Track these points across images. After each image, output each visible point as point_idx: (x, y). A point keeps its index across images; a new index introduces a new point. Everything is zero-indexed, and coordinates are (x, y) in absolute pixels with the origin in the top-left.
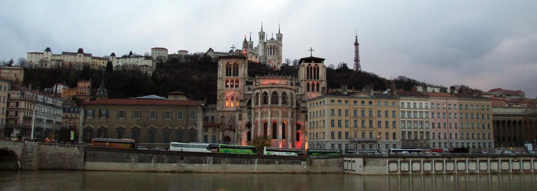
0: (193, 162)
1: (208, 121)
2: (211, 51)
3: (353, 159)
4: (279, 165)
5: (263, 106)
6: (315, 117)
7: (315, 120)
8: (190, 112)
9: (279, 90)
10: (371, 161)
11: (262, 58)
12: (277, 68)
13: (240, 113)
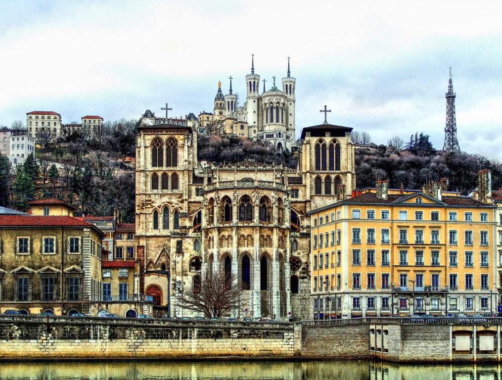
3: (385, 328)
4: (240, 340)
5: (242, 225)
6: (324, 245)
7: (324, 251)
8: (69, 239)
9: (252, 193)
11: (252, 129)
12: (284, 148)
13: (179, 239)
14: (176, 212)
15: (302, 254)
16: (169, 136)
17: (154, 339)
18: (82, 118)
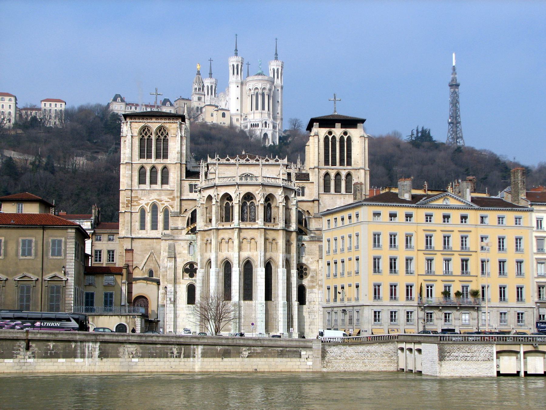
0: (56, 356)
1: (100, 261)
2: (119, 100)
3: (417, 346)
4: (252, 359)
5: (222, 227)
8: (50, 240)
9: (257, 190)
10: (457, 351)
14: (166, 212)
15: (311, 260)
16: (160, 124)
17: (152, 357)
18: (41, 101)
